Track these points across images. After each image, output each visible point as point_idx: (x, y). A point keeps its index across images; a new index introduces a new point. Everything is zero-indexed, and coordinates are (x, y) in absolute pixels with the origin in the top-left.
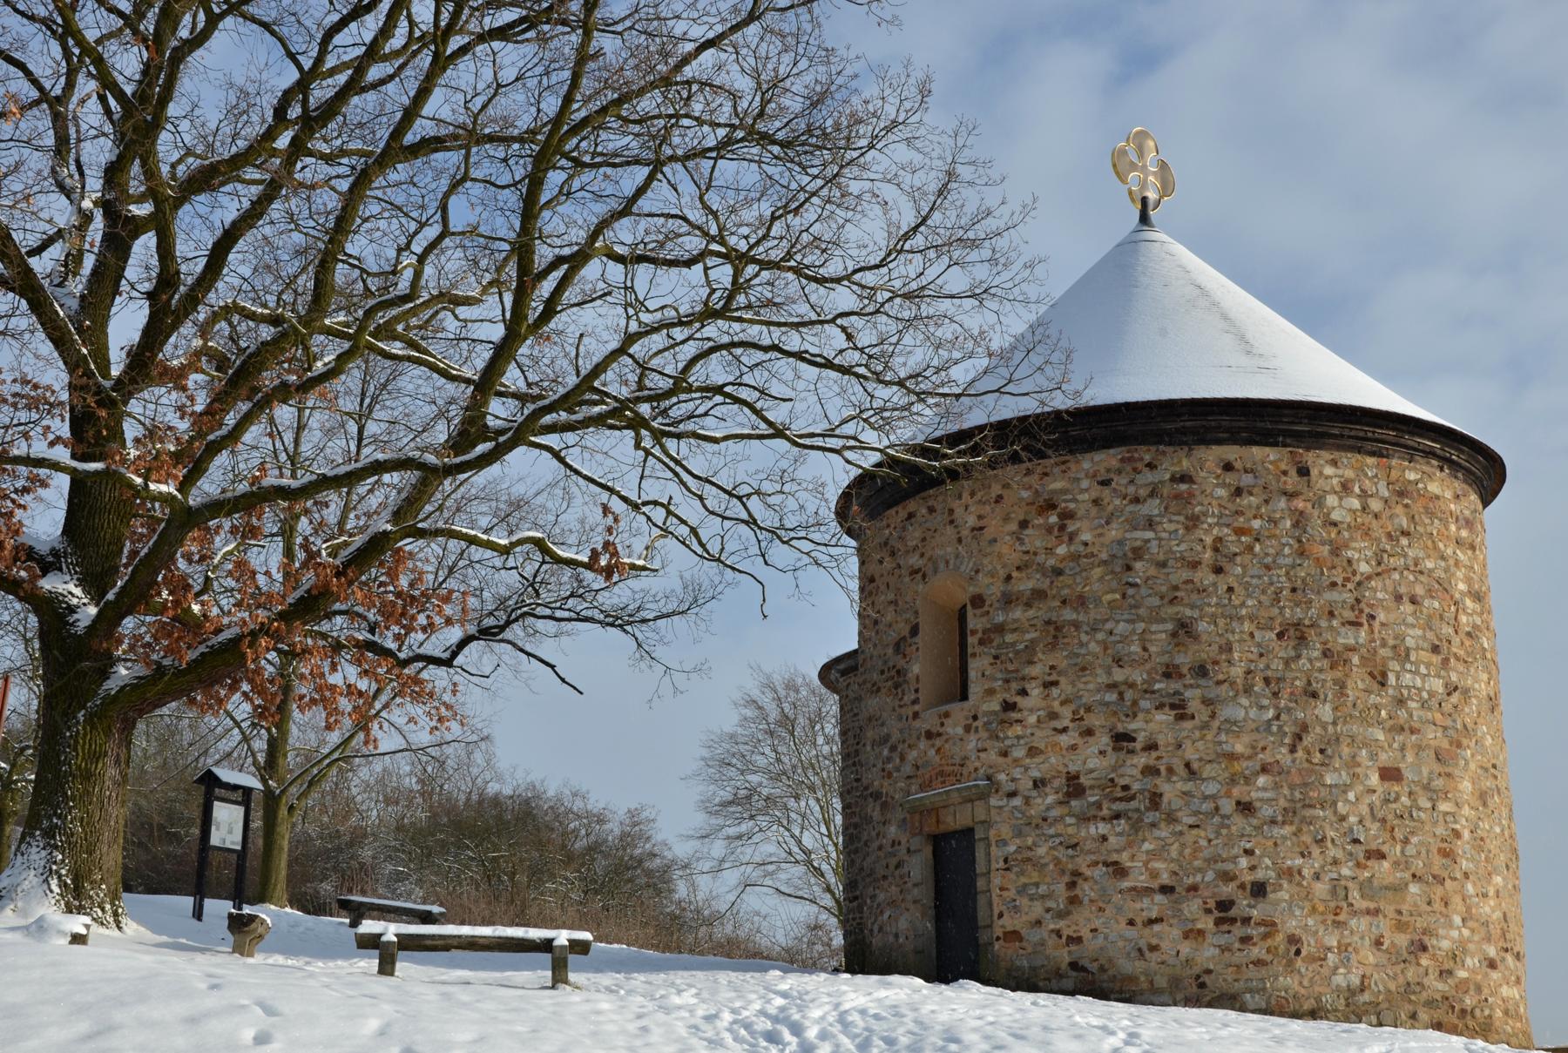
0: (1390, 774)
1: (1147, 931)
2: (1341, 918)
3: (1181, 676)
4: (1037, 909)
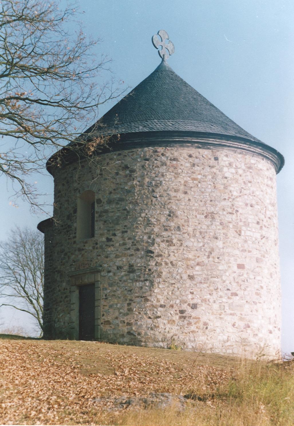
2: (221, 316)
4: (117, 314)
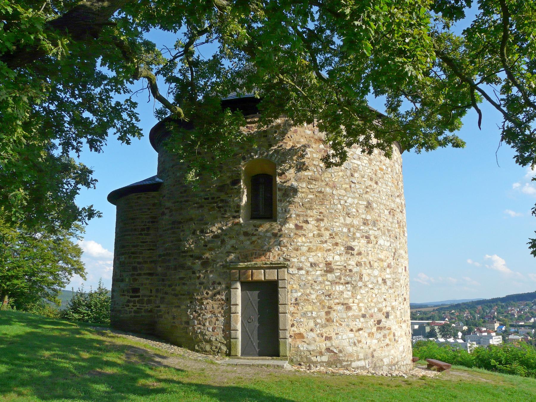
1: (357, 334)
3: (368, 224)
4: (312, 324)
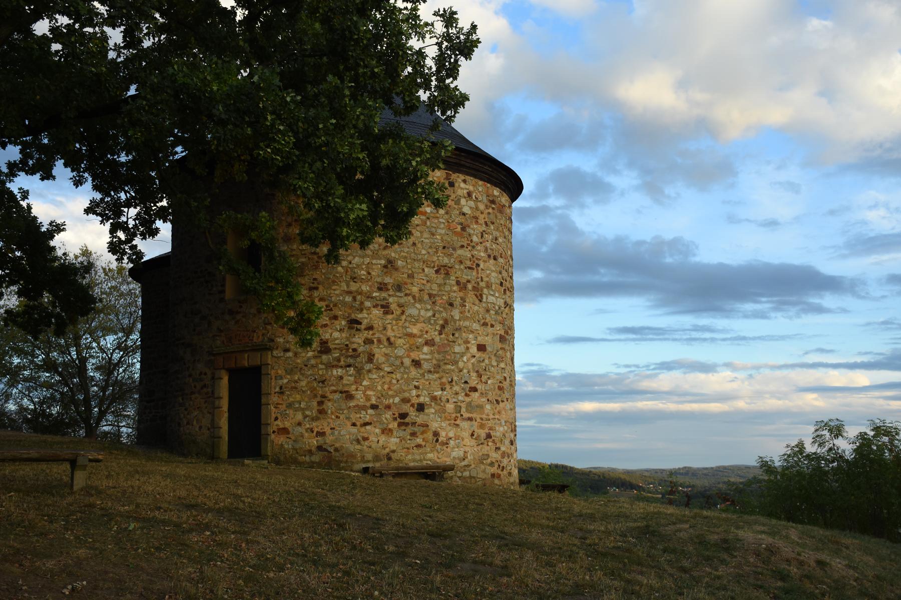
0: (481, 348)
1: (363, 429)
2: (457, 422)
4: (299, 416)
